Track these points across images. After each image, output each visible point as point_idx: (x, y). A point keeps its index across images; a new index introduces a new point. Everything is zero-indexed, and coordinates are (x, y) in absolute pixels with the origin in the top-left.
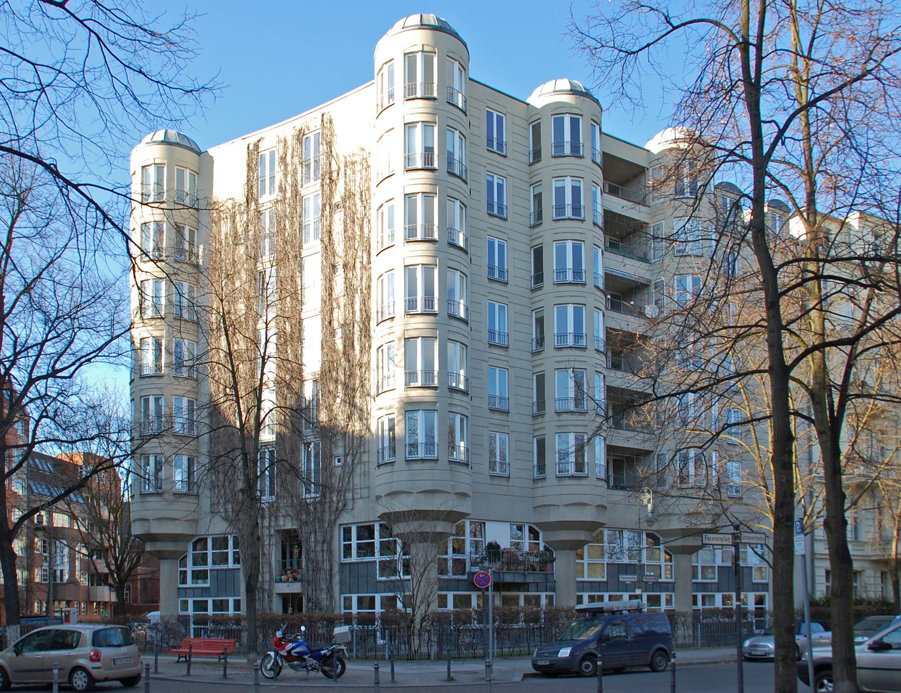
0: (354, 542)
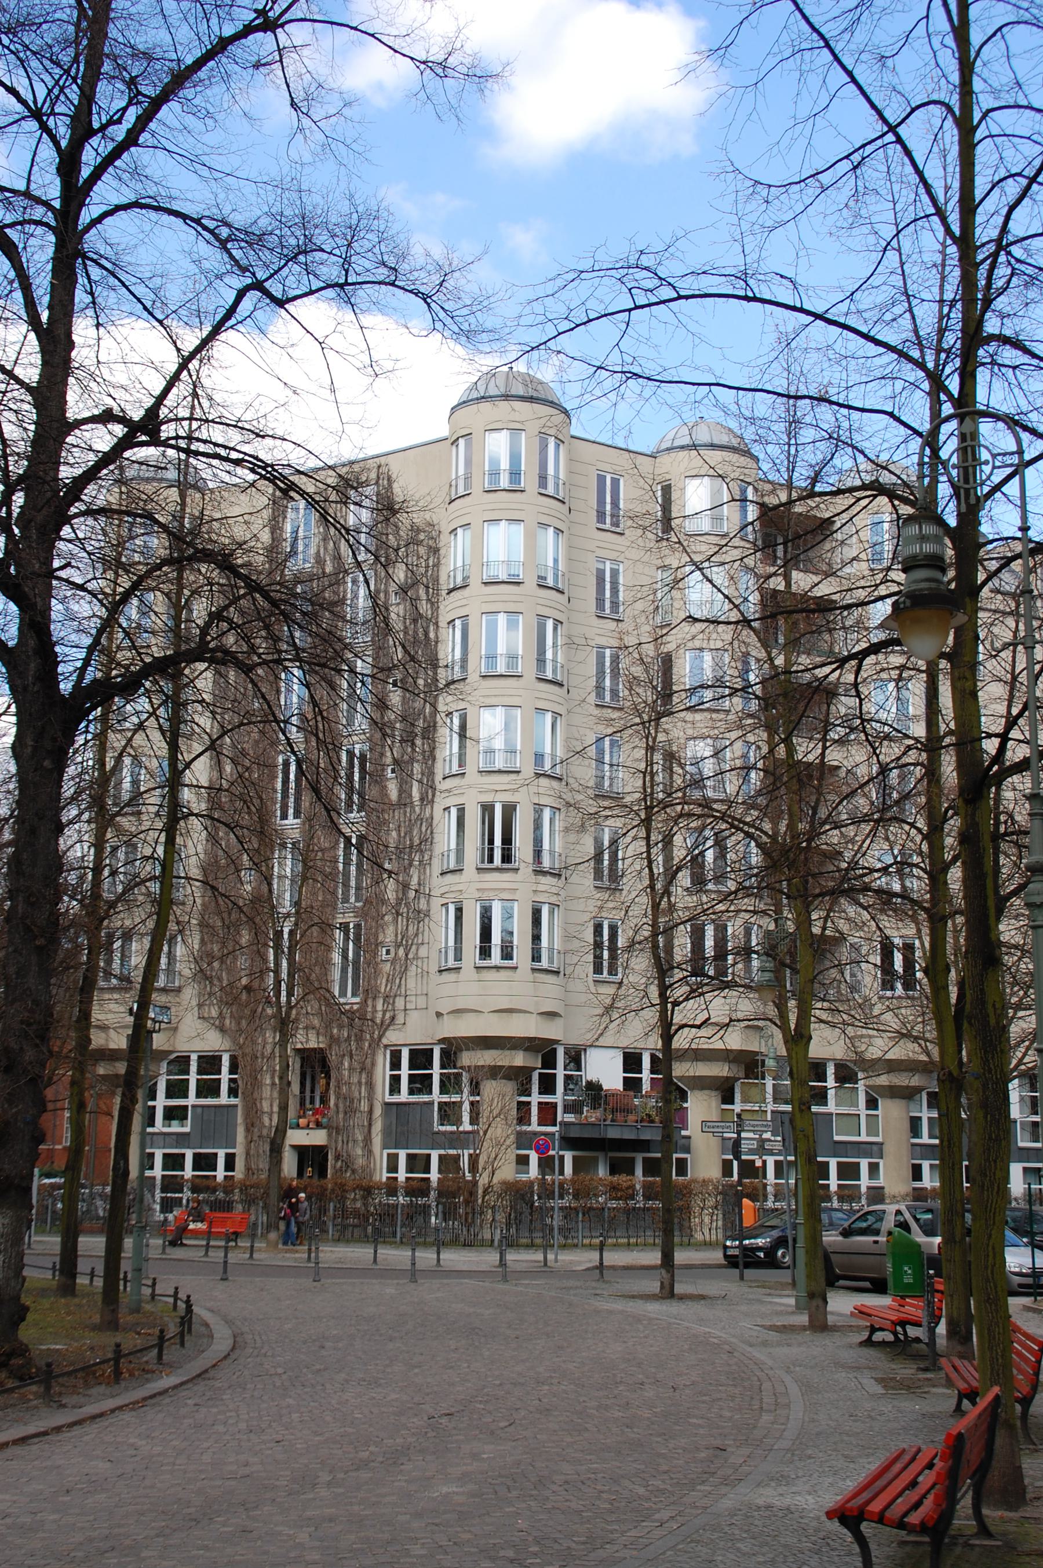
0: (405, 1072)
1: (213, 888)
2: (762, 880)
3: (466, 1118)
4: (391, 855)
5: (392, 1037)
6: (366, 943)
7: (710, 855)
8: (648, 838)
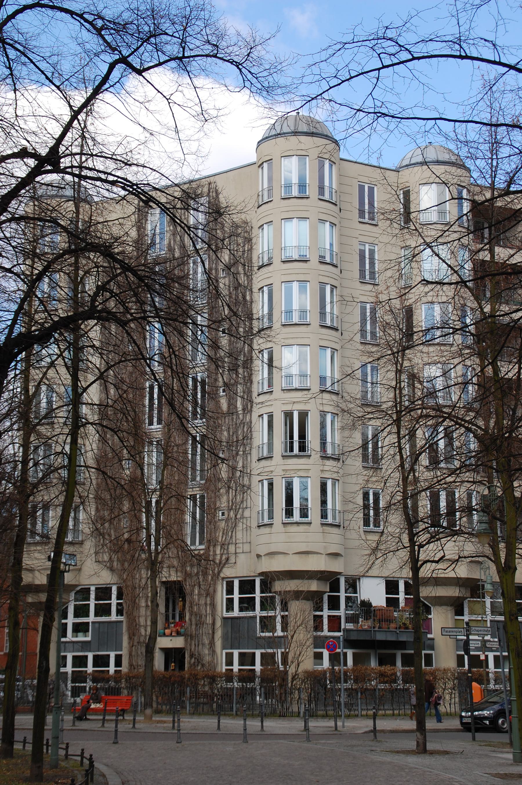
0: (236, 596)
1: (104, 473)
2: (478, 460)
3: (279, 627)
4: (224, 447)
5: (227, 572)
6: (208, 509)
7: (442, 444)
8: (398, 433)
